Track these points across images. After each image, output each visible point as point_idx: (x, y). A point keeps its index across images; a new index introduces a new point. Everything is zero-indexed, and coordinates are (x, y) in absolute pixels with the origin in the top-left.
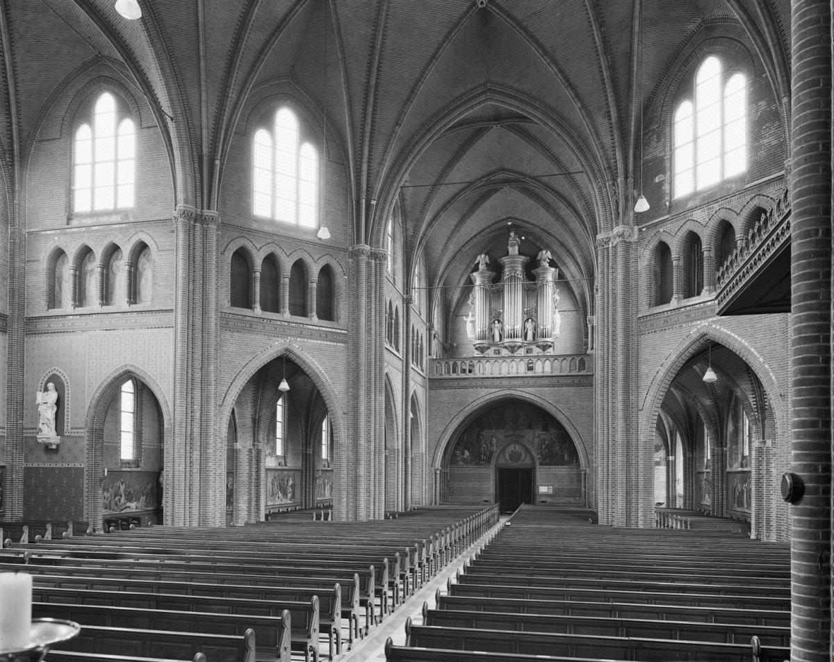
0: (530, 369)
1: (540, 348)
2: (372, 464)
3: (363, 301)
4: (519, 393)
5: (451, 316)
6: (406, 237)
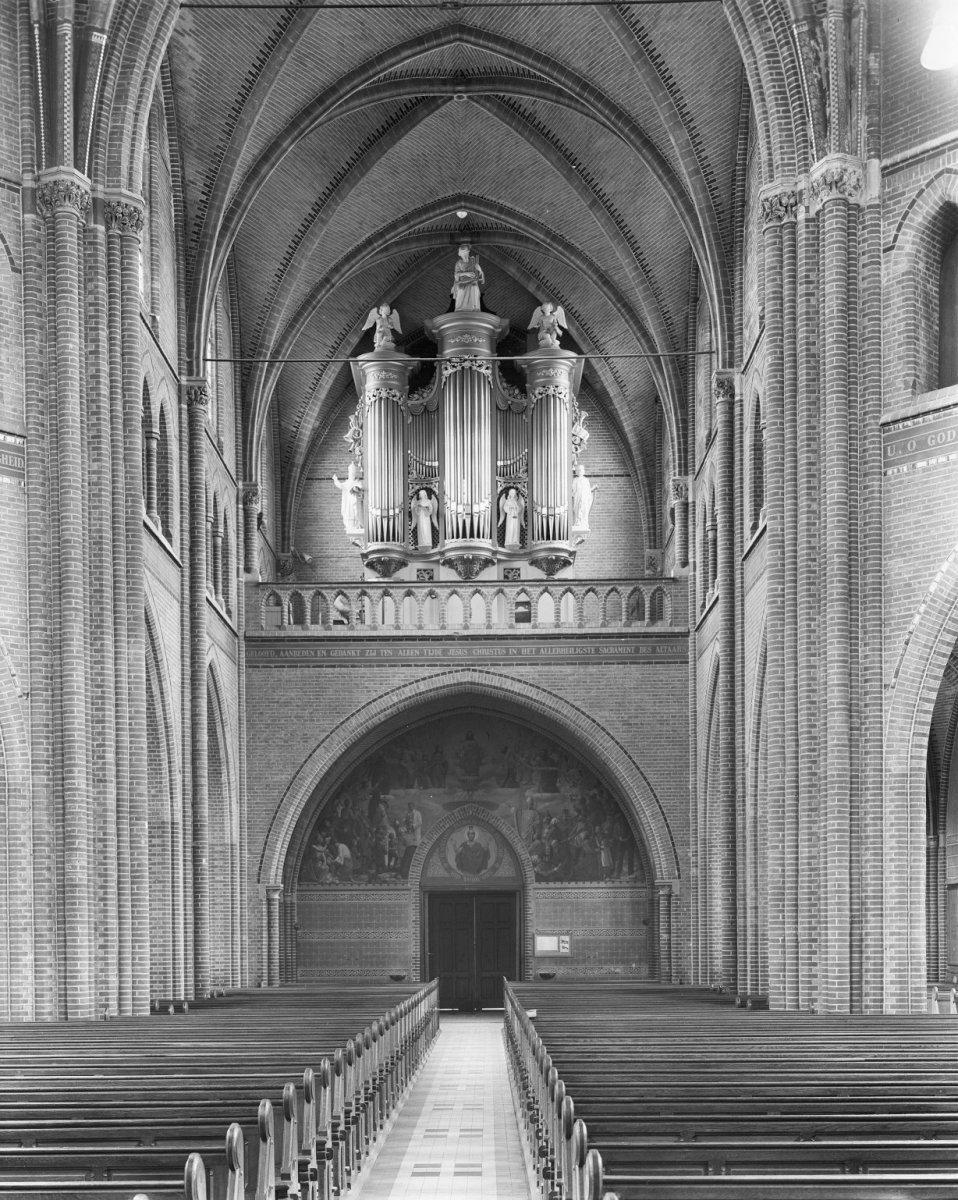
0: (524, 618)
1: (540, 567)
2: (112, 851)
3: (74, 345)
4: (496, 682)
5: (294, 472)
6: (183, 205)
